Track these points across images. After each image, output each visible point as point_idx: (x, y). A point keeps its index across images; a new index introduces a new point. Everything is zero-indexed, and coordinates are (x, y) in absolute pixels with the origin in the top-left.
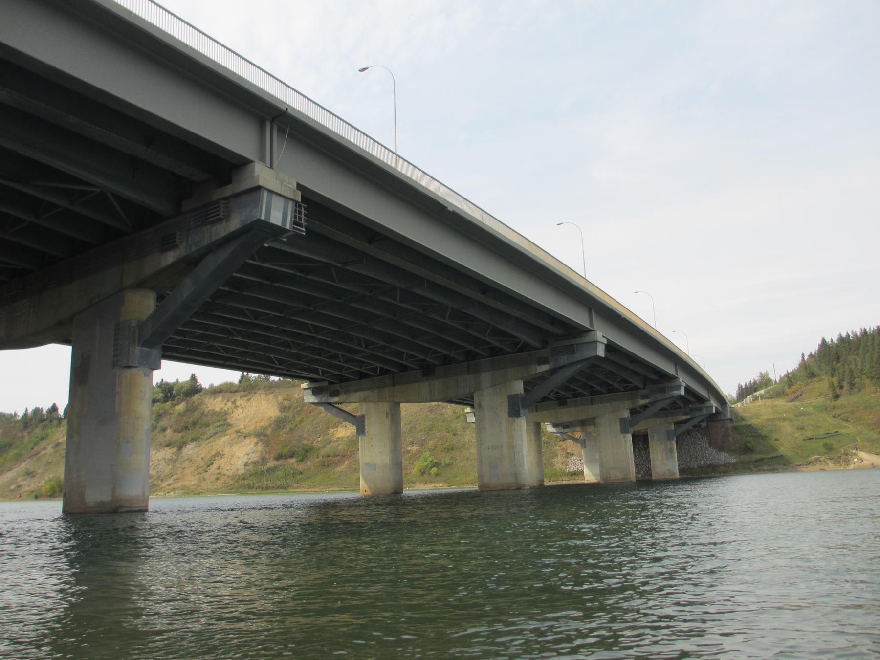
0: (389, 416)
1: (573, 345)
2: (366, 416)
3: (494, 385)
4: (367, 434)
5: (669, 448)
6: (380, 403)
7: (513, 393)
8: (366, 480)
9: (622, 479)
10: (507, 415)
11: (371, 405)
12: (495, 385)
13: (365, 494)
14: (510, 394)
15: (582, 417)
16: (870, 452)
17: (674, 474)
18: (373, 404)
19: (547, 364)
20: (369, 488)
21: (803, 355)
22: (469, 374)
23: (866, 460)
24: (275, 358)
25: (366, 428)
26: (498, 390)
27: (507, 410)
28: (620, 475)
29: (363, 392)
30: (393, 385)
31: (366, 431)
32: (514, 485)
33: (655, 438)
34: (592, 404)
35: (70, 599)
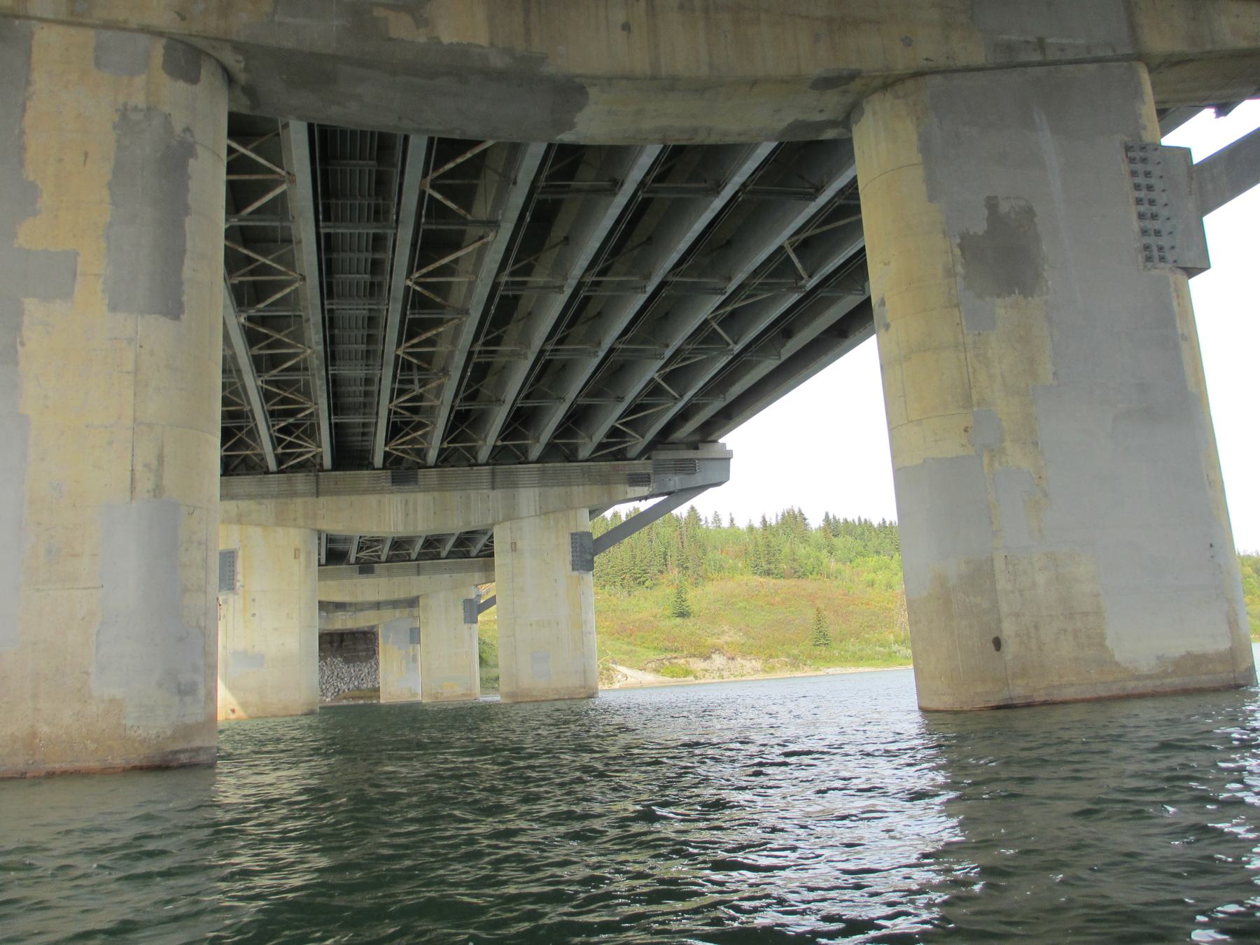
0: (303, 557)
1: (692, 460)
2: (240, 553)
3: (544, 512)
4: (241, 591)
5: (411, 654)
6: (280, 529)
7: (581, 529)
8: (232, 688)
9: (462, 695)
10: (569, 567)
11: (255, 532)
12: (546, 513)
13: (232, 716)
14: (574, 531)
15: (401, 594)
16: (631, 667)
17: (416, 694)
18: (259, 530)
19: (646, 486)
20: (244, 705)
21: (777, 515)
22: (493, 488)
23: (631, 677)
24: (464, 392)
25: (239, 577)
26: (552, 522)
27: (569, 558)
28: (459, 690)
29: (233, 503)
30: (318, 494)
31: (238, 584)
32: (582, 690)
33: (390, 640)
34: (418, 575)
35: (708, 872)
